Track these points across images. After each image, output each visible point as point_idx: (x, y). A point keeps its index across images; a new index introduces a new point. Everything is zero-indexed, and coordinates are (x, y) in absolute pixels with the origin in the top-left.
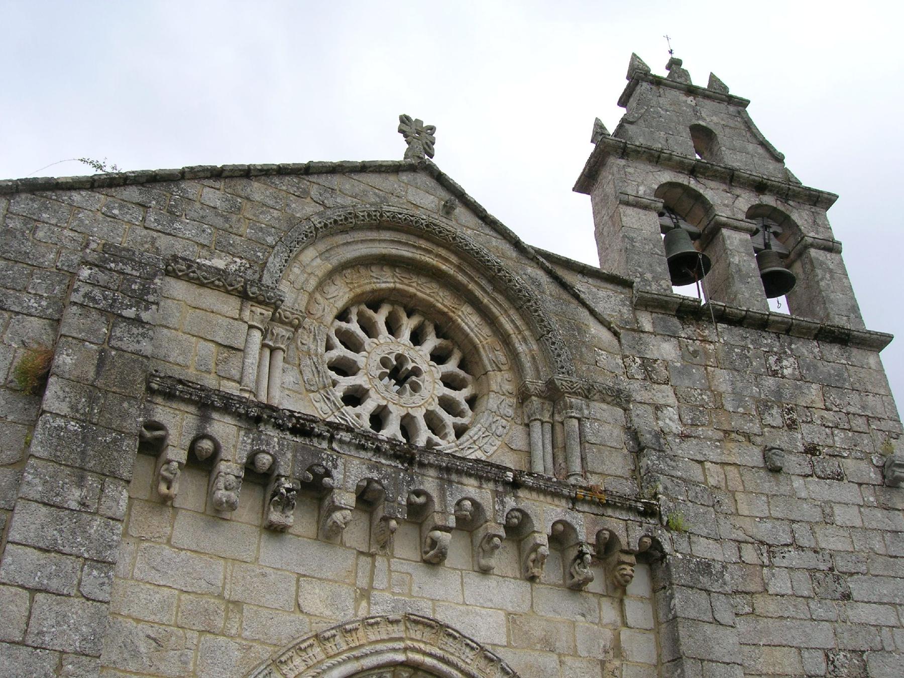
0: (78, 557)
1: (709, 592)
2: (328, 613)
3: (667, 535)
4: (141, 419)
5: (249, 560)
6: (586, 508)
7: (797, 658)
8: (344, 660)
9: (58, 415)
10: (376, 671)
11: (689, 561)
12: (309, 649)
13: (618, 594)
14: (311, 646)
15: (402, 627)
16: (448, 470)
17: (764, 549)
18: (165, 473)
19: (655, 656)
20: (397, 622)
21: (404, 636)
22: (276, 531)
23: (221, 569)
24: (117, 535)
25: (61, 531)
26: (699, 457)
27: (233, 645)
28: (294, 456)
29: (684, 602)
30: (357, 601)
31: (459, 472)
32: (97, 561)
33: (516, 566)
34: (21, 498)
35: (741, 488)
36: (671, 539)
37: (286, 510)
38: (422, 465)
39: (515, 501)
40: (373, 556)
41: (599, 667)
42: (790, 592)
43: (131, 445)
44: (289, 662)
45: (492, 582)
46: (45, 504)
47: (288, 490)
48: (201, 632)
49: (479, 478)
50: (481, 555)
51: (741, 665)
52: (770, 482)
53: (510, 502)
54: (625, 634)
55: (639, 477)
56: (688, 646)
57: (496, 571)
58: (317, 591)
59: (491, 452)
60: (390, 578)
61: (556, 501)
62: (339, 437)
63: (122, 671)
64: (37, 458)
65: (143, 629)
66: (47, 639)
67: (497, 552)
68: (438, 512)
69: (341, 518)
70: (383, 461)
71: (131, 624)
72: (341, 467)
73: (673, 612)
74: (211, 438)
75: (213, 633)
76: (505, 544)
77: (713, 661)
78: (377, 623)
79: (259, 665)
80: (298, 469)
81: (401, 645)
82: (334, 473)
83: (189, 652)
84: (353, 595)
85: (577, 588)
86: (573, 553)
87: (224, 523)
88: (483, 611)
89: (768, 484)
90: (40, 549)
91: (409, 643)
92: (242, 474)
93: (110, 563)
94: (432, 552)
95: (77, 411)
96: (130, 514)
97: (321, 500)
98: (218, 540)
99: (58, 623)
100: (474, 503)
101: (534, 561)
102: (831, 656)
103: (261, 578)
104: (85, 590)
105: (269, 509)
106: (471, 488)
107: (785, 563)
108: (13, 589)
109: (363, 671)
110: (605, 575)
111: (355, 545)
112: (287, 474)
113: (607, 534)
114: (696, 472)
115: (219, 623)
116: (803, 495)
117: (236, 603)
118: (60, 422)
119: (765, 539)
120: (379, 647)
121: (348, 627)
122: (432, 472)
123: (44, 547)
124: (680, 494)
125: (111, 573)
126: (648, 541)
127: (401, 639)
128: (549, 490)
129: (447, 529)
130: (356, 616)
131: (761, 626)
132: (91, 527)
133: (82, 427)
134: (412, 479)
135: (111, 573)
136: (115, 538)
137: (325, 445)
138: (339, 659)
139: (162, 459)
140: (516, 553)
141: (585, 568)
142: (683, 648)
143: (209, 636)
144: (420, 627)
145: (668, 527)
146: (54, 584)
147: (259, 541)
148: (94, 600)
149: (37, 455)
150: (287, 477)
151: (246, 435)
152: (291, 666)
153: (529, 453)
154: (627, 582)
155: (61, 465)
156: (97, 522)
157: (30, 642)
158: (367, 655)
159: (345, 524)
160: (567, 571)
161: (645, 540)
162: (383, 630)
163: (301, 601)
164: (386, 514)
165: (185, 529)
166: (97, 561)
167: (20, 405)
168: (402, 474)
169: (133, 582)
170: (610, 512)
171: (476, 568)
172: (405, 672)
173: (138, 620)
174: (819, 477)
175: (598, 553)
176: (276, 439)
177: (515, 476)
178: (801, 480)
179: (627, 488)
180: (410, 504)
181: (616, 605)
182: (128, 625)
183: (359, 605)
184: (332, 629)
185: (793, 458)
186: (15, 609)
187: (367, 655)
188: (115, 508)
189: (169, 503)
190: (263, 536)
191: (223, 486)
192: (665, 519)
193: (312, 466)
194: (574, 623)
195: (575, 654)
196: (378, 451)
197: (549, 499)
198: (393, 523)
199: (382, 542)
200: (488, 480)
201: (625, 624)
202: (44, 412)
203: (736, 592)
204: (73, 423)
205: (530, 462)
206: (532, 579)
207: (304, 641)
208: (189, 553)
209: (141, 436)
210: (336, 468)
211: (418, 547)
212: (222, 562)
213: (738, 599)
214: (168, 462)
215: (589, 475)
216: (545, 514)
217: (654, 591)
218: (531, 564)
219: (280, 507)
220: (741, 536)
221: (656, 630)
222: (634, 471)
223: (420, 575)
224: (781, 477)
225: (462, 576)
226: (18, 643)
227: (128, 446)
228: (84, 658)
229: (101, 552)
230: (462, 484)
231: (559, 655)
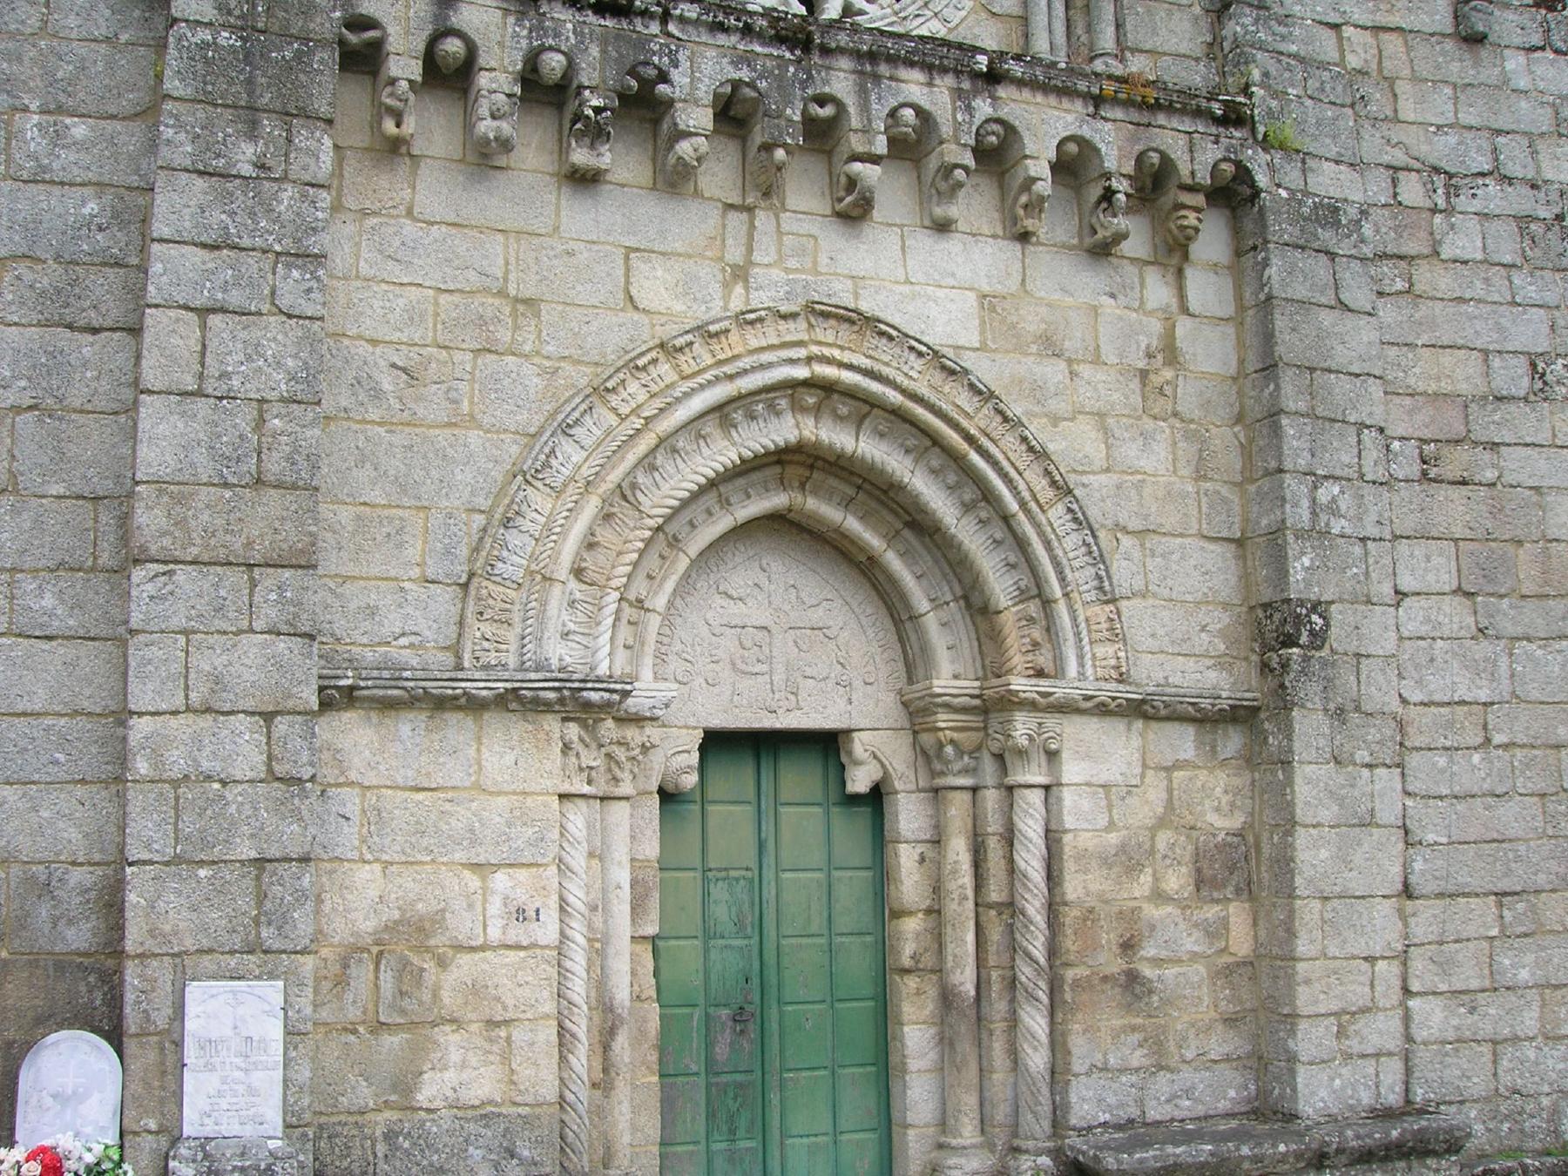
0: (265, 252)
1: (1332, 256)
2: (678, 307)
3: (1264, 157)
4: (338, 14)
5: (543, 231)
6: (1119, 113)
7: (1481, 368)
8: (709, 382)
9: (198, 22)
10: (763, 396)
11: (1300, 202)
12: (651, 367)
13: (1175, 261)
14: (654, 361)
15: (802, 324)
16: (872, 57)
17: (1439, 181)
18: (388, 101)
19: (1234, 363)
20: (793, 316)
21: (806, 338)
22: (584, 180)
23: (499, 249)
24: (323, 210)
25: (232, 214)
26: (1334, 18)
27: (528, 369)
28: (604, 52)
29: (1285, 272)
30: (727, 286)
31: (892, 60)
32: (297, 255)
33: (996, 215)
34: (161, 167)
35: (1406, 72)
36: (1271, 166)
37: (597, 145)
38: (826, 51)
39: (993, 105)
40: (750, 210)
41: (1137, 380)
42: (1479, 256)
43: (325, 60)
44: (621, 389)
45: (952, 245)
46: (201, 173)
47: (598, 110)
48: (477, 352)
49: (929, 68)
50: (935, 198)
51: (1380, 378)
52: (1461, 60)
53: (983, 108)
54: (1183, 327)
55: (1220, 55)
56: (1288, 344)
57: (961, 226)
58: (659, 273)
59: (957, 21)
60: (780, 243)
61: (1066, 103)
62: (678, 12)
63: (359, 422)
64: (176, 99)
65: (381, 357)
66: (235, 383)
67: (962, 193)
68: (856, 131)
69: (690, 150)
70: (758, 49)
71: (363, 349)
72: (685, 65)
73: (1266, 290)
74: (458, 34)
75: (496, 352)
76: (975, 179)
77: (1330, 371)
78: (761, 320)
79: (573, 396)
80: (611, 73)
81: (802, 353)
82: (675, 75)
83: (461, 385)
84: (720, 277)
85: (1102, 250)
86: (1096, 192)
87: (497, 173)
88: (940, 293)
89: (1458, 63)
90: (204, 246)
91: (815, 349)
92: (518, 90)
93: (316, 256)
94: (849, 199)
95: (229, 13)
96: (342, 175)
97: (656, 122)
98: (493, 202)
99: (249, 358)
100: (919, 111)
101: (1026, 207)
102: (1541, 366)
103: (566, 258)
104: (284, 302)
105: (569, 145)
106: (913, 87)
107: (1476, 205)
108: (172, 313)
109: (740, 397)
110: (1154, 228)
111: (717, 193)
112: (594, 83)
113: (1155, 158)
114: (1326, 46)
115: (504, 335)
116: (1523, 83)
117: (527, 302)
118: (205, 35)
119: (1443, 164)
120: (766, 357)
121: (713, 328)
122: (845, 63)
123: (210, 242)
124: (1293, 86)
125: (321, 272)
126: (1228, 168)
127: (800, 344)
128: (1052, 84)
129: (875, 159)
130: (726, 309)
131: (1421, 313)
132: (280, 202)
133: (241, 38)
134: (810, 77)
135: (321, 272)
136: (320, 215)
137: (655, 28)
138: (700, 380)
139: (383, 78)
140: (996, 193)
141: (1115, 216)
142: (1280, 350)
143: (491, 357)
144: (832, 322)
145: (1265, 144)
146: (235, 298)
147: (558, 199)
148: (300, 317)
149: (176, 94)
150: (592, 89)
151: (519, 22)
152: (625, 395)
153: (1025, 20)
154: (1189, 239)
155: (216, 105)
156: (289, 192)
157: (210, 391)
158: (745, 372)
159: (698, 160)
160: (1086, 221)
161: (1224, 166)
162: (770, 331)
163: (634, 292)
164: (767, 138)
165: (434, 189)
166: (297, 255)
167: (137, 13)
168: (792, 69)
169: (358, 283)
170: (1161, 119)
171: (927, 223)
172: (811, 395)
173: (374, 342)
174: (1557, 52)
175: (1140, 190)
176: (570, 26)
177: (991, 62)
178: (1521, 58)
179: (1197, 76)
180: (809, 122)
181: (1170, 278)
182: (360, 350)
183: (730, 293)
184: (687, 332)
185: (1511, 17)
186: (181, 342)
187: (745, 372)
188: (313, 167)
189: (403, 150)
190: (564, 189)
191: (487, 113)
192: (1261, 129)
193: (634, 67)
194: (1095, 309)
195: (1097, 361)
196: (747, 31)
197: (1053, 100)
198: (780, 154)
199: (764, 187)
200: (944, 70)
201: (1185, 310)
202: (175, 20)
203: (1384, 256)
204: (226, 34)
205: (1026, 36)
206: (1024, 237)
207: (643, 354)
208: (444, 228)
209: (342, 42)
210: (676, 67)
211: (827, 192)
212: (500, 237)
213: (1386, 268)
214: (393, 82)
215: (1128, 54)
216: (1045, 126)
217: (1238, 253)
218: (1021, 212)
219: (587, 140)
220: (1399, 157)
221: (1237, 320)
222: (1211, 45)
223: (832, 241)
224: (1485, 53)
225: (902, 236)
226: (192, 394)
227: (321, 62)
228: (295, 406)
229: (300, 240)
230: (898, 80)
231: (1070, 361)
